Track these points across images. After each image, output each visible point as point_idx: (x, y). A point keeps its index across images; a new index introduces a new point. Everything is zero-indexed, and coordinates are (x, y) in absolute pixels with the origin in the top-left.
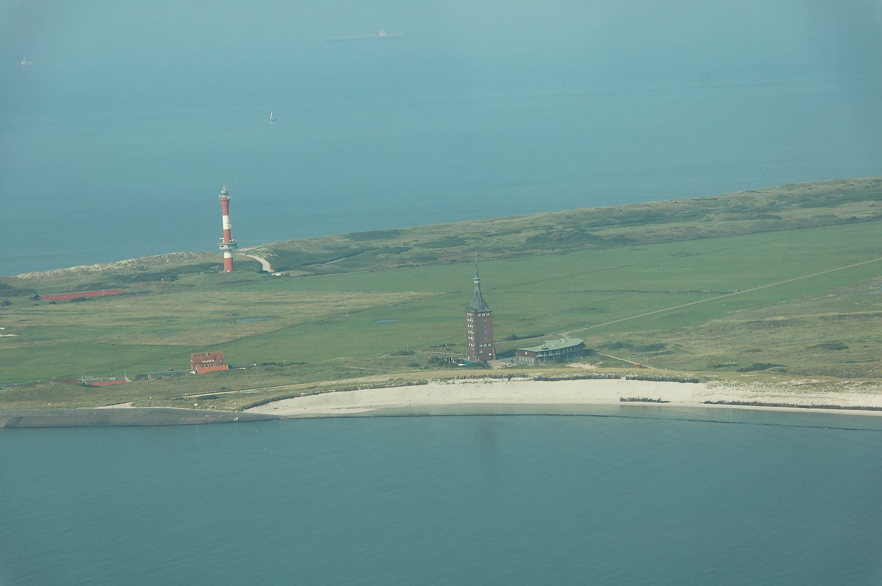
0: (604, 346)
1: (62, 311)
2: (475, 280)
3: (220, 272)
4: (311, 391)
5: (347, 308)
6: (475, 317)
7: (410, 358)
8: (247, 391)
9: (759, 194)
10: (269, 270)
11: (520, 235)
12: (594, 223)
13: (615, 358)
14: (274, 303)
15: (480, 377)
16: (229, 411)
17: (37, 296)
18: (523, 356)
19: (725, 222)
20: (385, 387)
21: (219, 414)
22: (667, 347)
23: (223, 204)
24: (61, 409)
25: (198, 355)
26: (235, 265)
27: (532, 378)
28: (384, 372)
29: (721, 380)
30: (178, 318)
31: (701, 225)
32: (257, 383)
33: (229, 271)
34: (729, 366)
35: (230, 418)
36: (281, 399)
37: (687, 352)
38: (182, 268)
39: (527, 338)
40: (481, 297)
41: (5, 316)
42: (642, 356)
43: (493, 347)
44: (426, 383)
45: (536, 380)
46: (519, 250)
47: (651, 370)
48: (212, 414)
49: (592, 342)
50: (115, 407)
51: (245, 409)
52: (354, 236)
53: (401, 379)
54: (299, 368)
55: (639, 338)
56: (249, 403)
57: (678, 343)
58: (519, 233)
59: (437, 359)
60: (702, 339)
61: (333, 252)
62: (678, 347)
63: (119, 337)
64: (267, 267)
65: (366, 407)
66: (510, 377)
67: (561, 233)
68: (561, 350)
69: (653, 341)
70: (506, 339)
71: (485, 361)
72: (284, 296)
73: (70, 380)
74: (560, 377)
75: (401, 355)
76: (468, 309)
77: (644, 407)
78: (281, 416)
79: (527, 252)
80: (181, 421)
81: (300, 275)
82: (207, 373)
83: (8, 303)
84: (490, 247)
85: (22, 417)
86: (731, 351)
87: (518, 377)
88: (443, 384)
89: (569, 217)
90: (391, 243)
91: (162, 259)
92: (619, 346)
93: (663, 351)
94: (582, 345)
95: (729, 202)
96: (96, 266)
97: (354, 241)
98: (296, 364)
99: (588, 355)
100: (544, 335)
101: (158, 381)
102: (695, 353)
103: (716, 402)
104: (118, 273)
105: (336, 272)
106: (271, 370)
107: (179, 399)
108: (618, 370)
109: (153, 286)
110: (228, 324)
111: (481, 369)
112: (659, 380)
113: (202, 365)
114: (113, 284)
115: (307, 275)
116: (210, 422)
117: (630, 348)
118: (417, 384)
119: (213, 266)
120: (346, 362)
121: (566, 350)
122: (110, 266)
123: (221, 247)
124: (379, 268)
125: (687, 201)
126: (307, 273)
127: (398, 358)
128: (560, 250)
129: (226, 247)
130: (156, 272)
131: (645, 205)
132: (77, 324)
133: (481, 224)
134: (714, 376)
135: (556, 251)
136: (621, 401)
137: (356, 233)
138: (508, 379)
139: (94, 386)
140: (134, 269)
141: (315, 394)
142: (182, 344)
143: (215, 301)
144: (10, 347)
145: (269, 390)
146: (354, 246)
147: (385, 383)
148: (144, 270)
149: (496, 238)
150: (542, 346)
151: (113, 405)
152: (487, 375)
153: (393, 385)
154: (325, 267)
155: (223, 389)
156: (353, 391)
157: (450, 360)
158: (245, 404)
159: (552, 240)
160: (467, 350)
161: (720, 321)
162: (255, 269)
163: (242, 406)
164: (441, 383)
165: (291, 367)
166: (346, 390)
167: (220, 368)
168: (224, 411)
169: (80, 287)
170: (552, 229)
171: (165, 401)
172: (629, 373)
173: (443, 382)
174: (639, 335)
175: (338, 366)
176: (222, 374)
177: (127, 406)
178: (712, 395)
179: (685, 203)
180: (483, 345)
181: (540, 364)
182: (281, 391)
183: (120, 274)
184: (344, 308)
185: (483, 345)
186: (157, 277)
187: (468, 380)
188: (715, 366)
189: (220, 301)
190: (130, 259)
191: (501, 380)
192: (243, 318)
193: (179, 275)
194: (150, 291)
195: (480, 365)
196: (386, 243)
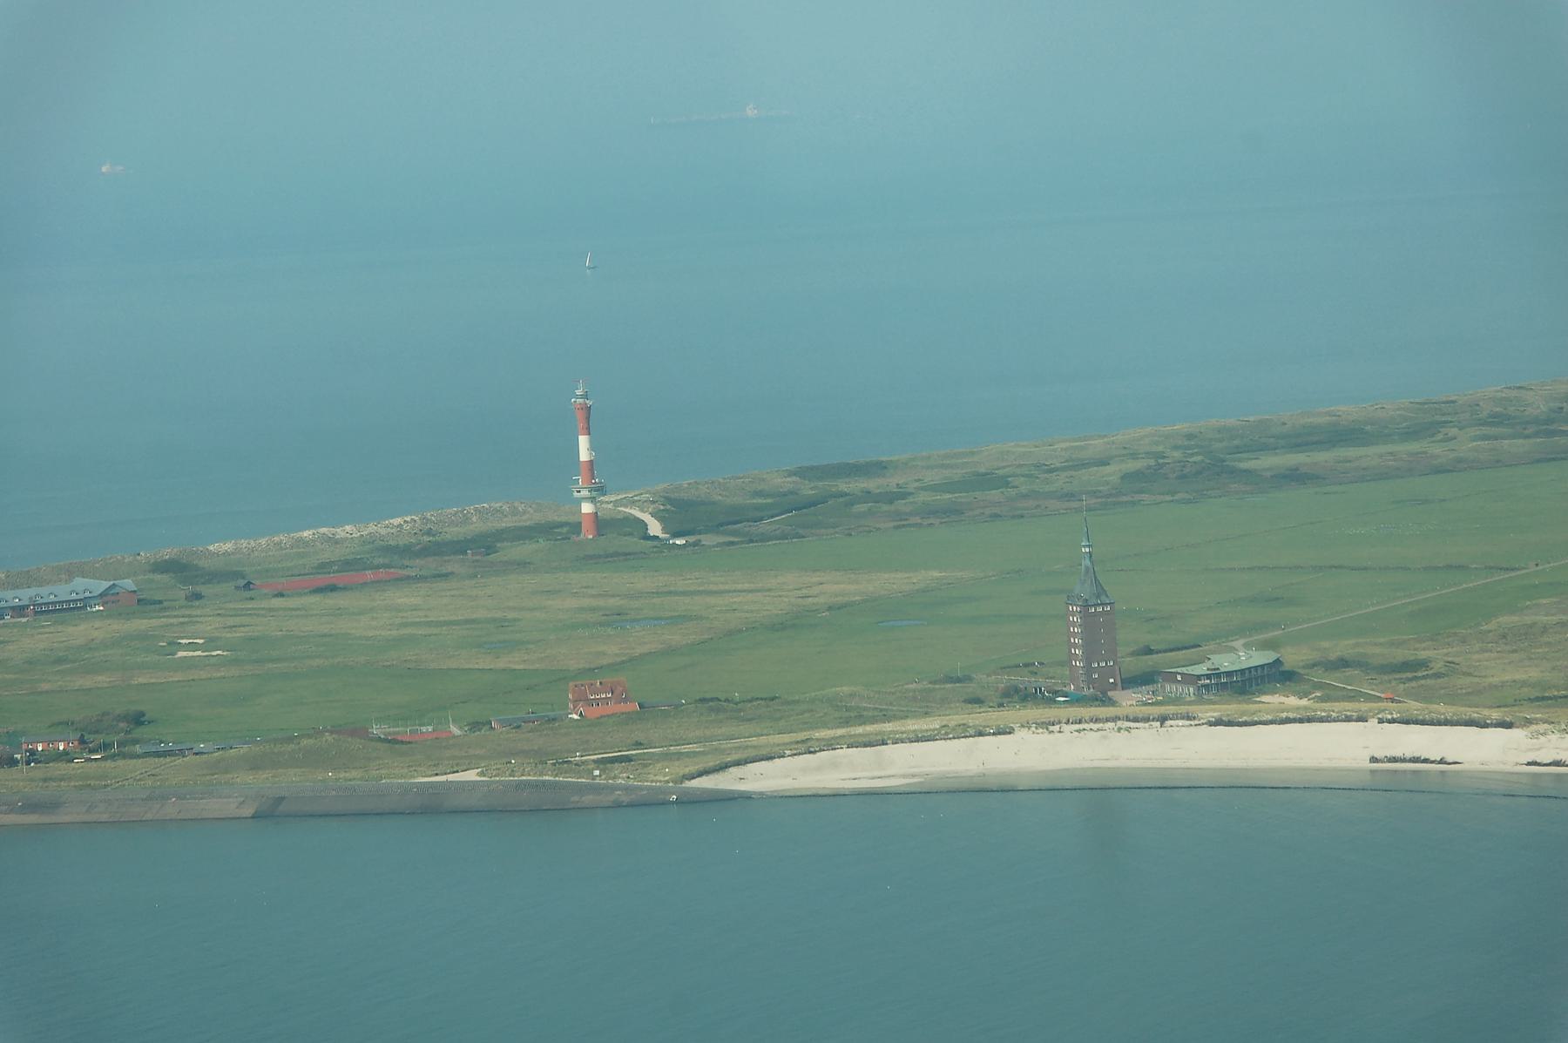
0: (1314, 665)
1: (298, 609)
2: (1084, 546)
3: (574, 537)
4: (802, 748)
5: (822, 600)
6: (1085, 614)
7: (965, 687)
8: (685, 749)
9: (1532, 393)
10: (661, 536)
11: (1108, 469)
12: (1237, 447)
13: (1340, 685)
14: (684, 593)
15: (1107, 720)
16: (658, 784)
17: (249, 583)
18: (1174, 682)
19: (1479, 443)
20: (937, 740)
21: (641, 788)
22: (1431, 665)
23: (580, 416)
24: (352, 783)
25: (582, 685)
26: (601, 524)
27: (1204, 721)
28: (926, 714)
29: (1553, 723)
30: (515, 620)
31: (1437, 450)
32: (698, 733)
33: (591, 537)
34: (1555, 698)
35: (662, 797)
36: (751, 762)
37: (1470, 674)
38: (503, 531)
39: (1165, 651)
40: (1095, 578)
41: (198, 619)
42: (1390, 681)
43: (1117, 668)
44: (1010, 732)
45: (1211, 724)
46: (1111, 495)
47: (1414, 707)
48: (627, 789)
49: (1293, 657)
50: (451, 777)
51: (687, 779)
52: (803, 473)
53: (964, 725)
54: (768, 706)
55: (1377, 650)
56: (692, 769)
57: (1450, 659)
58: (1105, 465)
59: (1017, 690)
60: (1491, 651)
61: (769, 501)
62: (1452, 665)
63: (417, 655)
64: (655, 528)
65: (904, 776)
66: (1163, 719)
67: (1182, 464)
68: (1242, 671)
69: (1401, 655)
70: (1133, 654)
71: (1104, 693)
72: (700, 580)
73: (360, 732)
74: (1256, 719)
75: (947, 682)
76: (1071, 599)
77: (1415, 772)
78: (755, 793)
79: (1125, 499)
80: (573, 802)
81: (718, 543)
82: (602, 717)
83: (198, 596)
84: (1056, 491)
85: (283, 798)
86: (1550, 672)
87: (1177, 719)
88: (1042, 733)
89: (1190, 436)
90: (873, 484)
91: (464, 515)
92: (1343, 664)
93: (1426, 672)
94: (1278, 662)
95: (1478, 408)
96: (348, 528)
97: (807, 482)
98: (762, 699)
99: (1290, 680)
100: (1200, 646)
101: (516, 732)
102: (1485, 677)
103: (1548, 762)
104: (387, 541)
105: (784, 537)
106: (718, 710)
107: (562, 765)
108: (1364, 706)
109: (454, 565)
110: (610, 631)
111: (1099, 706)
112: (1439, 723)
113: (589, 703)
114: (381, 560)
115: (732, 543)
116: (624, 804)
117: (1363, 669)
118: (994, 734)
119: (558, 527)
120: (852, 695)
121: (1250, 672)
122: (372, 528)
123: (576, 494)
124: (861, 529)
125: (1402, 406)
126: (732, 539)
127: (944, 688)
128: (1187, 496)
129: (585, 493)
130: (455, 539)
131: (1329, 414)
132: (333, 632)
133: (1032, 450)
134: (1538, 716)
135: (1177, 497)
136: (1370, 762)
137: (807, 468)
138: (1159, 723)
139: (402, 742)
140: (415, 533)
141: (810, 752)
142: (537, 666)
143: (575, 591)
144: (223, 674)
145: (722, 746)
146: (808, 489)
147: (936, 732)
148: (434, 536)
149: (1065, 474)
150: (1208, 664)
151: (446, 774)
152: (1121, 717)
153: (951, 736)
154: (765, 526)
155: (638, 745)
156: (879, 747)
157: (1040, 689)
158: (687, 771)
159: (1167, 478)
160: (1068, 673)
161: (1515, 618)
162: (635, 533)
163: (681, 774)
164: (1038, 731)
165: (754, 706)
166: (865, 746)
167: (623, 708)
168: (649, 784)
169: (323, 567)
170: (1164, 457)
171: (540, 767)
172: (1383, 711)
173: (1041, 730)
174: (1376, 644)
175: (839, 704)
176: (629, 718)
177: (471, 776)
178: (1539, 749)
179: (1398, 409)
180: (1099, 664)
181: (1205, 697)
182: (747, 747)
183: (391, 543)
184: (816, 600)
185: (1099, 664)
186: (459, 547)
187: (1086, 725)
188: (1530, 699)
189: (585, 590)
190: (406, 516)
191: (1147, 725)
192: (634, 621)
193: (498, 545)
194: (452, 573)
195: (1097, 700)
196: (865, 485)
